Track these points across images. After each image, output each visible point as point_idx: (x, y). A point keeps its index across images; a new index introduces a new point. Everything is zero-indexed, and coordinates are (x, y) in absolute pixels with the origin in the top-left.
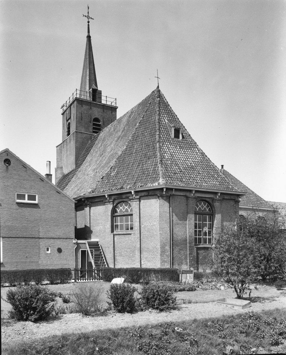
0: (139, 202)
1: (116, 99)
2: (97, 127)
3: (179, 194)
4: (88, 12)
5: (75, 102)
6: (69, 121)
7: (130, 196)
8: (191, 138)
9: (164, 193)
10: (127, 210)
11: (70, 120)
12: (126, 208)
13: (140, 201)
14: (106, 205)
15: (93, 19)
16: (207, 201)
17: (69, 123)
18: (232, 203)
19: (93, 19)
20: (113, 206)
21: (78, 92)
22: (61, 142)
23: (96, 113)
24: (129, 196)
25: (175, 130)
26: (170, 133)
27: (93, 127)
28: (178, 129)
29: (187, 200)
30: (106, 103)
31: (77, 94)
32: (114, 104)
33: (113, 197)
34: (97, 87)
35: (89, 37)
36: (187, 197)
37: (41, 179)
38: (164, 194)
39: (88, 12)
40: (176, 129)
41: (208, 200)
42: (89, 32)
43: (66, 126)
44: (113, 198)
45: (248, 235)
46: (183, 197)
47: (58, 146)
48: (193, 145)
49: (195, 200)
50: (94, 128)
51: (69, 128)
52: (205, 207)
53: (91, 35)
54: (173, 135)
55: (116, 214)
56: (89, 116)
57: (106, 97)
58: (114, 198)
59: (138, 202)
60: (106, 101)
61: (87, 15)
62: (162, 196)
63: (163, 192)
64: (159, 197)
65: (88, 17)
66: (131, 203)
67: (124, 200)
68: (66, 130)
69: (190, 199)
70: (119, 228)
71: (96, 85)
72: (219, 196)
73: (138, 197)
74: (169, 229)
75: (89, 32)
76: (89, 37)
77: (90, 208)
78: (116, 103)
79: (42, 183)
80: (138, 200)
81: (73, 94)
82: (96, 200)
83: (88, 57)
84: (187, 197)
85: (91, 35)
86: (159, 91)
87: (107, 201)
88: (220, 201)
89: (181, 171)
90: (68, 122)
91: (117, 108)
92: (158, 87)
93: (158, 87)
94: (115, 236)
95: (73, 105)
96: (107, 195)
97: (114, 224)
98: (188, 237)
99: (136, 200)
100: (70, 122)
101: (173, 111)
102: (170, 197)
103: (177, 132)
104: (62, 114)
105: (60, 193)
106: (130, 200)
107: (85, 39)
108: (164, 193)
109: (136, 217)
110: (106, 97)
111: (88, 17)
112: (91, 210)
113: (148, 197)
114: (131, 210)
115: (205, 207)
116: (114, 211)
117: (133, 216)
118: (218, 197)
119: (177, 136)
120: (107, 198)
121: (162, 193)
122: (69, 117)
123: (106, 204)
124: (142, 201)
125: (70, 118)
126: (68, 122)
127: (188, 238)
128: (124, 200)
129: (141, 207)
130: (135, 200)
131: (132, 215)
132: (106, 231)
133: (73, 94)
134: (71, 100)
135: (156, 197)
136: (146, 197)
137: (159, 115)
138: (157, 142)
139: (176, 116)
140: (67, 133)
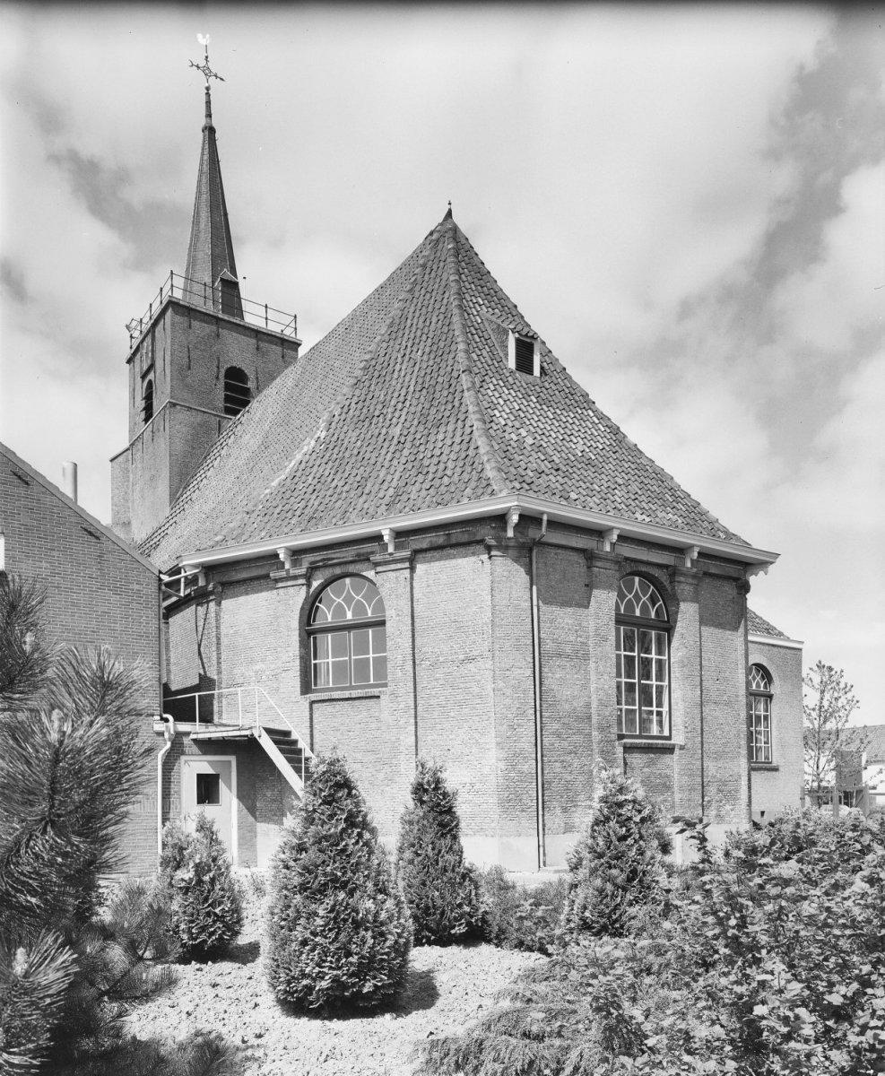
0: (408, 570)
1: (295, 317)
2: (237, 393)
3: (563, 542)
4: (207, 57)
5: (169, 313)
6: (151, 376)
7: (372, 553)
8: (568, 377)
9: (510, 533)
10: (359, 609)
11: (152, 372)
12: (358, 600)
13: (412, 569)
14: (281, 591)
15: (222, 79)
16: (653, 576)
17: (150, 381)
18: (730, 590)
19: (222, 79)
20: (308, 592)
21: (179, 282)
22: (127, 445)
23: (238, 353)
24: (369, 550)
25: (518, 341)
26: (501, 355)
27: (226, 407)
28: (529, 340)
29: (589, 567)
30: (265, 326)
31: (172, 286)
32: (288, 332)
33: (307, 560)
34: (236, 276)
35: (210, 131)
36: (590, 556)
37: (20, 477)
38: (509, 539)
39: (207, 57)
40: (523, 341)
41: (656, 573)
42: (209, 115)
43: (140, 393)
44: (305, 565)
45: (817, 686)
46: (575, 557)
47: (120, 454)
48: (580, 401)
49: (617, 568)
50: (227, 399)
51: (149, 398)
52: (644, 599)
53: (214, 125)
54: (512, 363)
55: (318, 623)
56: (210, 362)
57: (266, 307)
58: (312, 563)
59: (407, 573)
60: (266, 319)
61: (202, 63)
62: (504, 547)
63: (506, 531)
64: (489, 549)
65: (207, 72)
66: (378, 579)
67: (351, 569)
68: (141, 404)
69: (599, 564)
70: (341, 659)
71: (233, 270)
72: (692, 561)
73: (406, 553)
74: (529, 672)
75: (209, 115)
76: (210, 131)
77: (219, 604)
78: (296, 329)
79: (22, 491)
80: (407, 565)
81: (161, 289)
82: (244, 575)
83: (205, 189)
84: (590, 556)
85: (215, 125)
86: (455, 229)
87: (283, 574)
88: (695, 582)
89: (555, 467)
90: (146, 381)
91: (300, 345)
92: (449, 214)
93: (449, 214)
94: (315, 706)
95: (162, 322)
96: (287, 548)
97: (313, 662)
98: (594, 705)
99: (399, 566)
100: (153, 380)
101: (501, 290)
102: (531, 550)
103: (526, 348)
104: (129, 362)
105: (97, 538)
106: (376, 564)
107: (199, 137)
108: (510, 533)
109: (397, 627)
110: (266, 307)
111: (207, 72)
112: (222, 614)
113: (445, 552)
114: (380, 606)
115: (644, 599)
116: (309, 611)
117: (388, 624)
118: (689, 564)
119: (524, 364)
120: (283, 563)
121: (502, 534)
122: (149, 362)
123: (280, 585)
124: (420, 568)
125: (152, 367)
126: (146, 381)
127: (593, 711)
128: (351, 569)
129: (416, 591)
130: (393, 567)
131: (383, 623)
132: (282, 690)
133: (161, 289)
134: (157, 309)
135: (480, 548)
136: (436, 554)
137: (460, 294)
138: (463, 372)
139: (516, 306)
140: (143, 415)
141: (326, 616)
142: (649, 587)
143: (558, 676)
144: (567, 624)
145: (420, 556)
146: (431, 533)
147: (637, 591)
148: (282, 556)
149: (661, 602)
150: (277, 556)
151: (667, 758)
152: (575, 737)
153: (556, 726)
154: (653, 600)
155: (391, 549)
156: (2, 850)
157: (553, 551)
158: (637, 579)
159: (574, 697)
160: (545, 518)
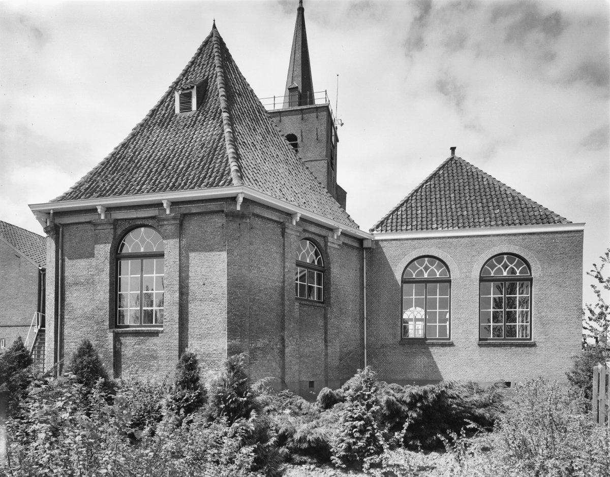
12: (148, 242)
41: (318, 239)
52: (311, 253)
92: (214, 27)
96: (167, 200)
141: (128, 249)
142: (314, 247)
143: (75, 295)
144: (82, 265)
145: (187, 218)
146: (183, 205)
147: (308, 249)
148: (165, 205)
149: (320, 256)
150: (162, 204)
151: (155, 340)
152: (85, 329)
153: (72, 323)
154: (316, 254)
155: (168, 212)
156: (259, 476)
157: (75, 227)
158: (308, 242)
159: (85, 306)
160: (52, 212)
